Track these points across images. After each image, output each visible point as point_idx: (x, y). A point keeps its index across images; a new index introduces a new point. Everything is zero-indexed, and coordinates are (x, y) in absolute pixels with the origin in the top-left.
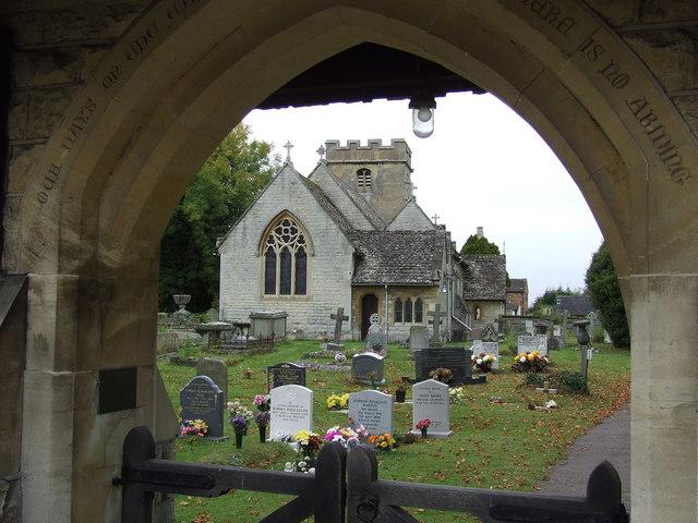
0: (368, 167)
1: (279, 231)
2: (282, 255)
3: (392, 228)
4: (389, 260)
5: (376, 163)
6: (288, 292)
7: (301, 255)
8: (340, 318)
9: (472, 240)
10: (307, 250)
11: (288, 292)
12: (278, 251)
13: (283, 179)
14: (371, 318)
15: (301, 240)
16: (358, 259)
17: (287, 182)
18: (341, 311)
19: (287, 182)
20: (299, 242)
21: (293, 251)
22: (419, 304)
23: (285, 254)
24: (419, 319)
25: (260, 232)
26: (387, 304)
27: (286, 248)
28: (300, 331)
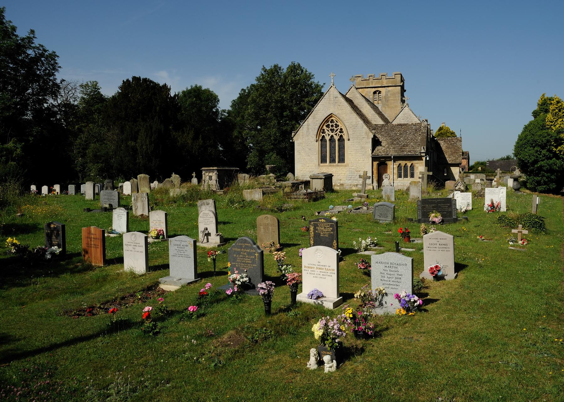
0: (380, 89)
1: (328, 126)
2: (330, 140)
3: (395, 123)
4: (394, 141)
5: (385, 87)
6: (326, 162)
7: (341, 139)
8: (365, 177)
9: (441, 129)
10: (345, 137)
11: (326, 162)
12: (328, 138)
13: (330, 96)
14: (384, 176)
15: (341, 131)
16: (376, 143)
17: (332, 97)
18: (366, 173)
19: (332, 97)
20: (340, 132)
21: (336, 138)
22: (412, 167)
23: (332, 139)
24: (412, 176)
25: (317, 127)
26: (392, 167)
27: (332, 136)
28: (342, 185)
